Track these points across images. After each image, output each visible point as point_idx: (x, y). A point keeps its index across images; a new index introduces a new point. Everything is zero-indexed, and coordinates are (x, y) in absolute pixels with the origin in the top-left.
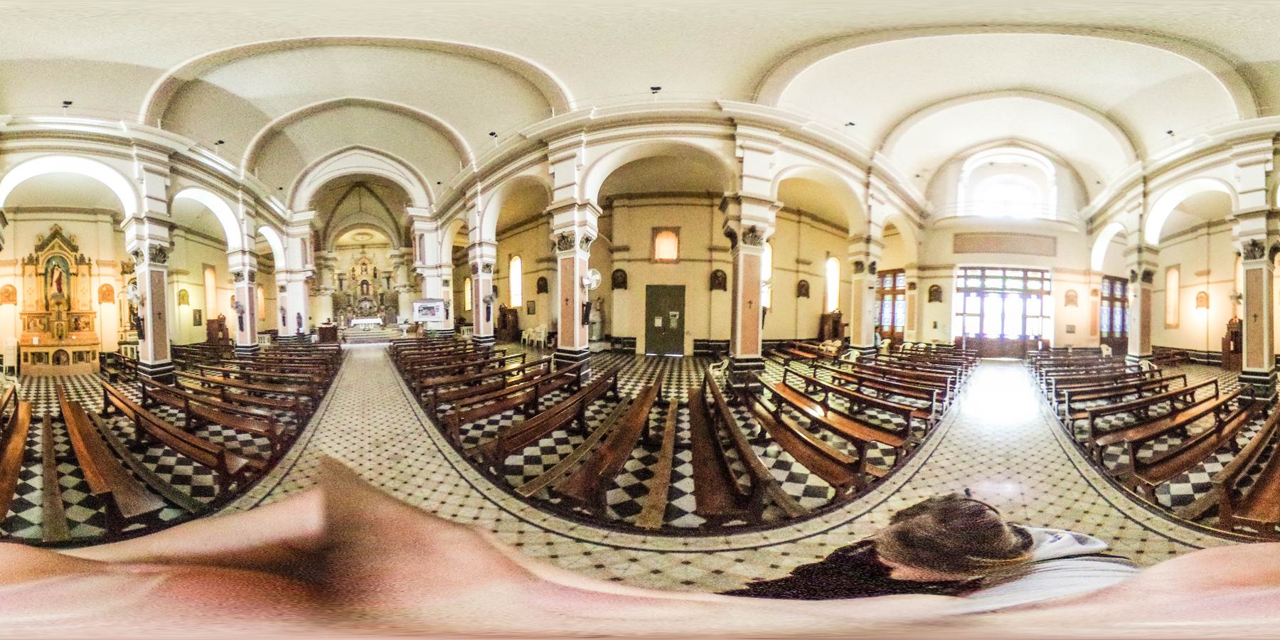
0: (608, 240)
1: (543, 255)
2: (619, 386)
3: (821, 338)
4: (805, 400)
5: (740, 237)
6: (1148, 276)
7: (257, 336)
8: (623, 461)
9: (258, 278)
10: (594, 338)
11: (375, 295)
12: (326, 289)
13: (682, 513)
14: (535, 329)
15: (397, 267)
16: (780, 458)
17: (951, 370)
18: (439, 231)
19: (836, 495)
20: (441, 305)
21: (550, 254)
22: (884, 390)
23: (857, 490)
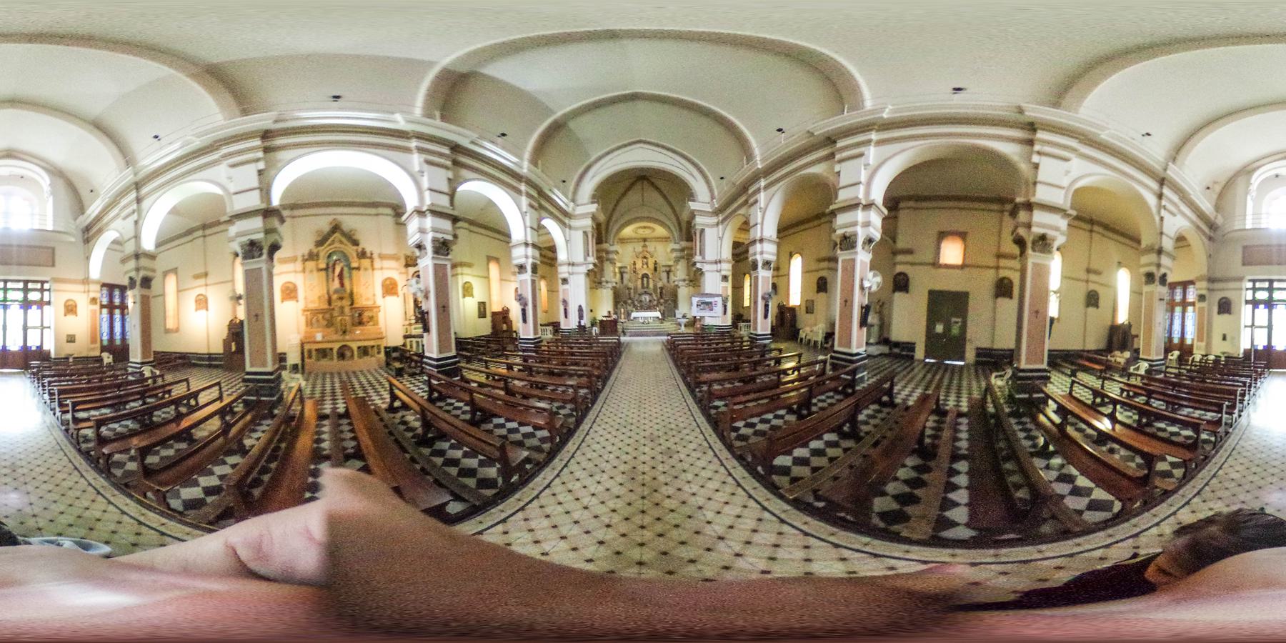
0: (891, 242)
1: (824, 253)
2: (895, 391)
3: (1109, 349)
4: (1092, 412)
5: (1029, 245)
6: (146, 282)
7: (539, 327)
8: (896, 469)
9: (540, 272)
10: (872, 341)
11: (655, 286)
12: (607, 282)
13: (954, 524)
14: (813, 329)
15: (677, 260)
16: (1064, 471)
17: (1241, 382)
18: (720, 227)
19: (1122, 509)
20: (719, 300)
21: (831, 254)
22: (1173, 403)
23: (1145, 503)
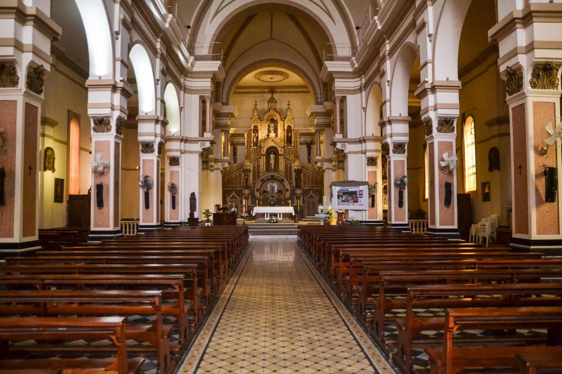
11: (288, 168)
12: (216, 161)
18: (364, 93)
20: (365, 188)
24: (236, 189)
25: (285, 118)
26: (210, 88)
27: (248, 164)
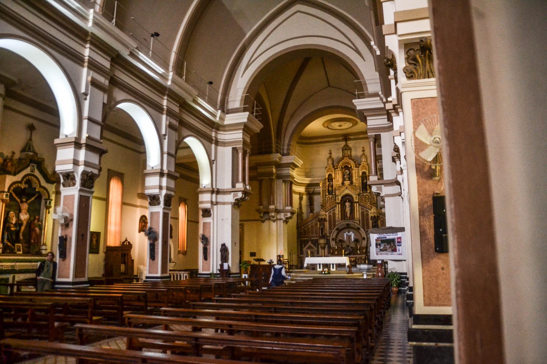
11: (364, 215)
12: (277, 211)
24: (312, 238)
25: (360, 165)
26: (242, 139)
27: (324, 213)
